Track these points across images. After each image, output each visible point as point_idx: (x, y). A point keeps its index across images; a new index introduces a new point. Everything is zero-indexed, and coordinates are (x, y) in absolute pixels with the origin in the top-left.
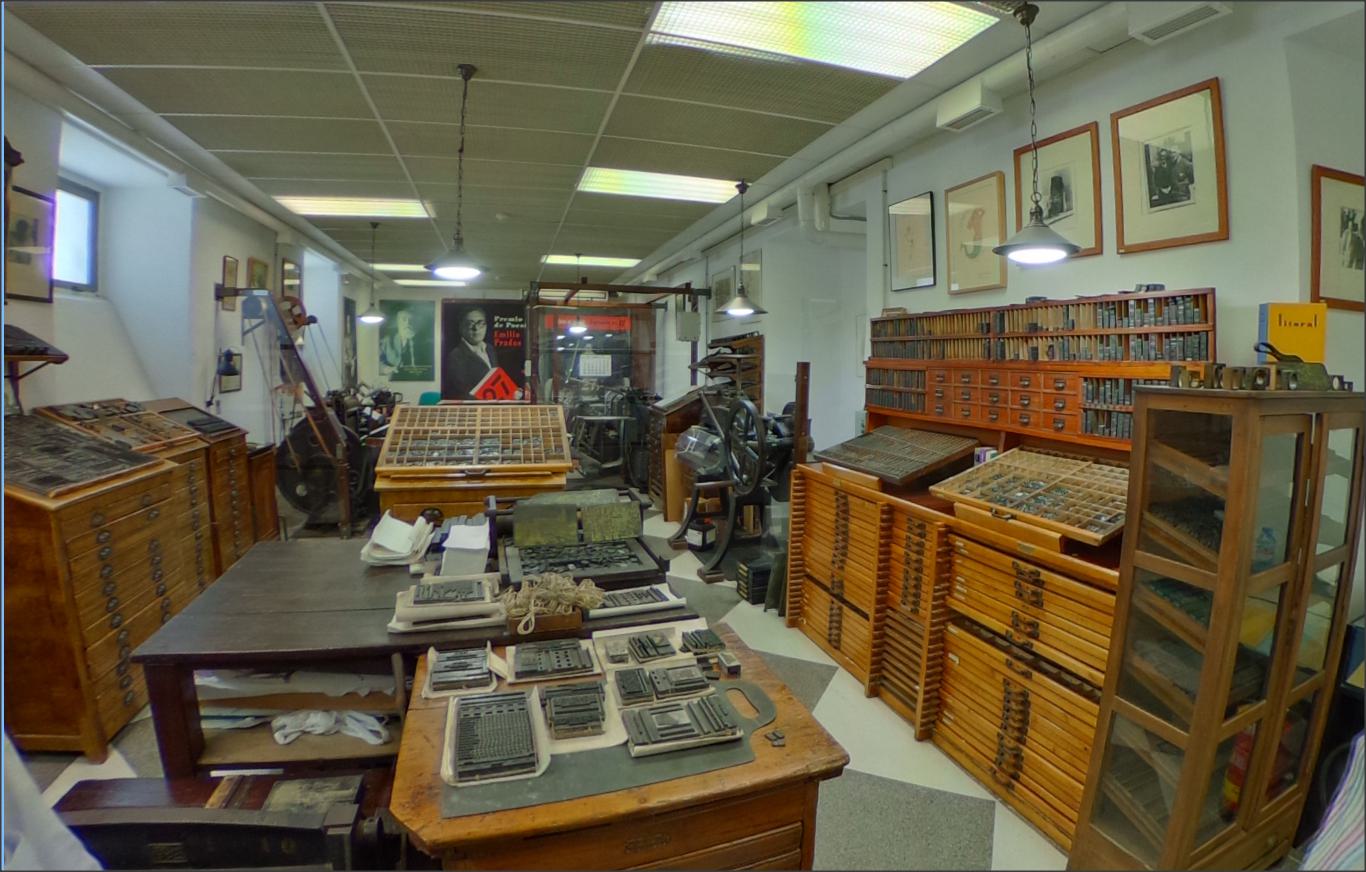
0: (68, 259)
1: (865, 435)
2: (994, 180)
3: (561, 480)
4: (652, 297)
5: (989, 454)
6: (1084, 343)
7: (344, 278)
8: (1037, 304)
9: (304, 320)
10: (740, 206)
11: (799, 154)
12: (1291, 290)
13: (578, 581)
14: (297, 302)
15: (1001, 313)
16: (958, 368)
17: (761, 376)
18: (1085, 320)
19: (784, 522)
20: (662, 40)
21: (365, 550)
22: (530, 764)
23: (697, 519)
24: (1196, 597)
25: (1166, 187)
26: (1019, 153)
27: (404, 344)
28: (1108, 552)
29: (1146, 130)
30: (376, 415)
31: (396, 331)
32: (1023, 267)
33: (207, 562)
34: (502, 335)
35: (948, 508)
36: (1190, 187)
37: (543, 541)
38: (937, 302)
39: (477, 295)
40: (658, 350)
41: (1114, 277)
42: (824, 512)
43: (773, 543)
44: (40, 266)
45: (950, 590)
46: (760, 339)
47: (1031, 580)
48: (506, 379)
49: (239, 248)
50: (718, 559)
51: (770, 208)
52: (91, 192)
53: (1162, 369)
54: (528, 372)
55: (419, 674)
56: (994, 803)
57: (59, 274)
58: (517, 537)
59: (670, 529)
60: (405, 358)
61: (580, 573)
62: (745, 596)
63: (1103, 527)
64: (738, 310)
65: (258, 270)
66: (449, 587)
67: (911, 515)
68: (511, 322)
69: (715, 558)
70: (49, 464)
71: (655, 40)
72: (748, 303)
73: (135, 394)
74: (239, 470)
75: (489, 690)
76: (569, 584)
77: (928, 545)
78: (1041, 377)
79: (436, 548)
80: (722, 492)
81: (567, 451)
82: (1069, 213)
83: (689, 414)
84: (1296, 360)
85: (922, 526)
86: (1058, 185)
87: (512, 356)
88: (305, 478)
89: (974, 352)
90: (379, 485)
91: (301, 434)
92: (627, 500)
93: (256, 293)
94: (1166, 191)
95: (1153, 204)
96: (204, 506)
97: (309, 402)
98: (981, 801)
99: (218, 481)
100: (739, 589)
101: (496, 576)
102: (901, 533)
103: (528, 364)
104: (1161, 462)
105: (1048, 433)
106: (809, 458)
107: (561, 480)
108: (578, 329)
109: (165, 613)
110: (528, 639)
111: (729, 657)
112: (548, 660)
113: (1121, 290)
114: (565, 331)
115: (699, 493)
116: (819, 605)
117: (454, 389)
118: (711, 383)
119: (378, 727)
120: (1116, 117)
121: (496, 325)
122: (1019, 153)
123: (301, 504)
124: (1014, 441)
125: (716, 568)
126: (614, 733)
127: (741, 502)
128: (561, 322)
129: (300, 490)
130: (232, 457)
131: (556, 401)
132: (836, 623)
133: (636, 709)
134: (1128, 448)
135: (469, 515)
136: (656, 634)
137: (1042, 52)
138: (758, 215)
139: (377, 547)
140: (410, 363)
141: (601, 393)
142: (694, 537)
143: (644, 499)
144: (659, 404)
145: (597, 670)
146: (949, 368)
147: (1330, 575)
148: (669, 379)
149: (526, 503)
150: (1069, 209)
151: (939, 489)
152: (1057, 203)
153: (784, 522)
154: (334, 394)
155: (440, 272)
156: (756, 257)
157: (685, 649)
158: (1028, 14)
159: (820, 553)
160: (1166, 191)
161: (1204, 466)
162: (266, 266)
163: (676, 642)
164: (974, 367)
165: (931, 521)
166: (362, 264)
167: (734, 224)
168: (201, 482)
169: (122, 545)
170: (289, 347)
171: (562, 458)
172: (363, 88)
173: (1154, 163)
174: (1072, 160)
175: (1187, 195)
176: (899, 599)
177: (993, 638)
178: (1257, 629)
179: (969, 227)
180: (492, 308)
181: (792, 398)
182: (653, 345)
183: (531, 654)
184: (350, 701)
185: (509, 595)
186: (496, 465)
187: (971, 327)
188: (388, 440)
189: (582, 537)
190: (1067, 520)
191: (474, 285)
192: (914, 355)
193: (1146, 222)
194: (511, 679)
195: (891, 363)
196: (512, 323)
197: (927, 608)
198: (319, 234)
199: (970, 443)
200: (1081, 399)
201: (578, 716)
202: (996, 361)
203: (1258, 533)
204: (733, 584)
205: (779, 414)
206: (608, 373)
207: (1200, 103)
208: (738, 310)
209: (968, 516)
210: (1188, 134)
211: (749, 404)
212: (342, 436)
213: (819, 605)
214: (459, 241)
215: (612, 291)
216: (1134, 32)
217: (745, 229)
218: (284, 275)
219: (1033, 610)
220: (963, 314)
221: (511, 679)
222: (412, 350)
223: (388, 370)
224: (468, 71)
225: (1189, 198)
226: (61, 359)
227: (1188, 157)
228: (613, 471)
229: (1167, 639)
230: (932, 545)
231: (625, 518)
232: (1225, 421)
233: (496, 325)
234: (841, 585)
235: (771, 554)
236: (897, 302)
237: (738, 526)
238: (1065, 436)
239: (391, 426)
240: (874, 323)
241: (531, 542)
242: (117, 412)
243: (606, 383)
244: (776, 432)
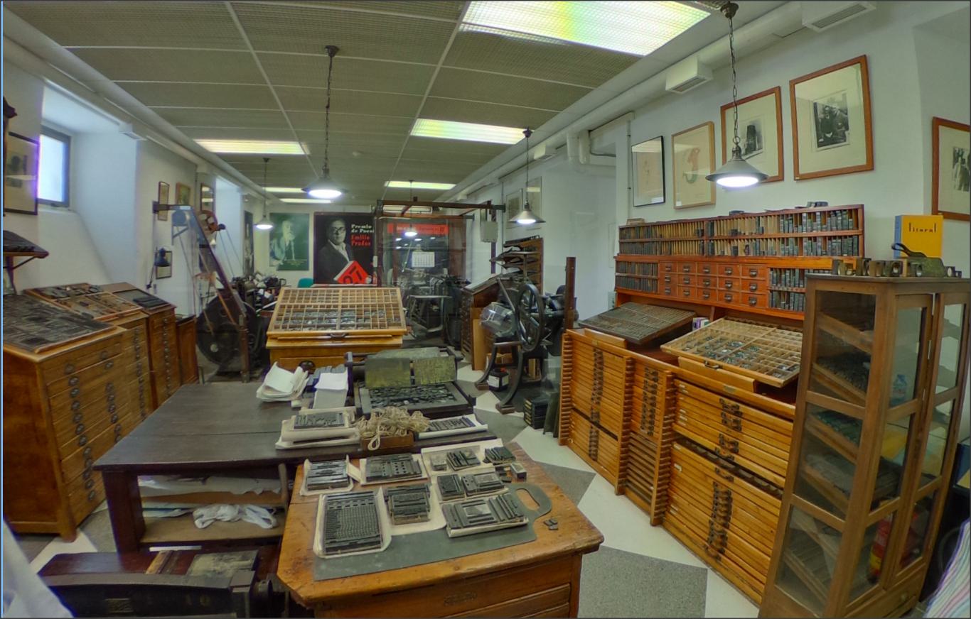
0: (48, 184)
1: (615, 308)
2: (706, 128)
3: (399, 341)
4: (464, 210)
5: (703, 322)
6: (770, 244)
7: (244, 197)
8: (737, 215)
9: (216, 227)
12: (918, 206)
13: (411, 412)
14: (211, 214)
15: (712, 222)
16: (681, 261)
17: (541, 267)
18: (771, 227)
19: (557, 371)
20: (471, 28)
21: (260, 390)
22: (377, 542)
23: (496, 369)
25: (829, 133)
26: (724, 108)
27: (287, 244)
28: (788, 392)
29: (815, 92)
30: (267, 295)
31: (282, 235)
32: (727, 190)
33: (147, 399)
34: (357, 238)
35: (674, 360)
36: (846, 133)
37: (386, 384)
38: (666, 214)
39: (339, 210)
40: (468, 248)
41: (792, 197)
42: (586, 363)
43: (550, 385)
44: (29, 189)
45: (675, 419)
46: (540, 240)
47: (733, 412)
48: (360, 269)
49: (170, 176)
50: (510, 397)
52: (65, 136)
53: (826, 262)
54: (375, 264)
55: (298, 478)
56: (706, 570)
57: (42, 194)
58: (368, 381)
59: (476, 376)
60: (288, 254)
61: (412, 406)
62: (530, 423)
63: (784, 374)
64: (524, 220)
65: (183, 192)
66: (319, 417)
67: (648, 366)
68: (363, 229)
69: (509, 396)
70: (35, 329)
71: (466, 28)
72: (531, 215)
73: (96, 280)
74: (170, 333)
75: (348, 490)
76: (404, 414)
77: (659, 387)
78: (740, 268)
79: (310, 389)
80: (513, 350)
81: (403, 320)
82: (760, 151)
83: (490, 294)
84: (921, 255)
85: (655, 373)
86: (752, 131)
87: (364, 253)
88: (217, 340)
89: (692, 250)
90: (269, 344)
91: (214, 308)
92: (446, 355)
94: (829, 135)
95: (820, 145)
96: (145, 359)
97: (219, 285)
98: (698, 569)
99: (155, 341)
100: (525, 418)
101: (353, 409)
102: (641, 378)
103: (375, 258)
104: (825, 328)
105: (745, 307)
106: (575, 325)
107: (399, 341)
108: (411, 234)
109: (117, 435)
110: (375, 453)
111: (518, 466)
112: (390, 469)
113: (797, 206)
114: (402, 235)
115: (497, 350)
116: (582, 430)
117: (323, 276)
118: (505, 272)
119: (268, 516)
120: (793, 83)
121: (353, 231)
122: (724, 108)
123: (214, 357)
124: (721, 313)
125: (509, 403)
126: (437, 520)
127: (527, 357)
128: (399, 228)
129: (214, 348)
130: (165, 324)
131: (395, 284)
132: (594, 442)
133: (452, 503)
134: (802, 318)
135: (334, 365)
136: (466, 450)
137: (740, 37)
138: (539, 152)
139: (268, 388)
140: (292, 258)
141: (427, 279)
142: (493, 381)
143: (458, 354)
144: (469, 287)
145: (424, 476)
146: (675, 261)
148: (475, 269)
149: (374, 357)
150: (760, 148)
151: (668, 347)
152: (751, 144)
153: (557, 371)
154: (237, 279)
155: (313, 193)
156: (538, 182)
157: (487, 461)
158: (731, 10)
159: (583, 392)
160: (829, 135)
161: (856, 331)
163: (481, 456)
165: (661, 369)
166: (258, 187)
167: (522, 159)
168: (143, 342)
169: (87, 387)
170: (205, 246)
171: (399, 325)
172: (258, 63)
173: (821, 116)
174: (762, 113)
175: (844, 138)
176: (639, 425)
177: (706, 453)
179: (689, 161)
180: (349, 219)
181: (563, 283)
182: (464, 245)
183: (377, 464)
184: (249, 498)
185: (362, 422)
186: (353, 330)
187: (691, 232)
188: (275, 312)
189: (413, 382)
190: (758, 369)
191: (337, 202)
192: (650, 252)
193: (814, 157)
194: (363, 482)
195: (633, 257)
196: (364, 229)
197: (659, 432)
198: (227, 166)
199: (690, 314)
200: (768, 283)
201: (411, 508)
202: (708, 257)
203: (894, 378)
204: (521, 415)
205: (554, 294)
206: (432, 265)
208: (524, 220)
209: (688, 366)
210: (844, 95)
211: (533, 287)
212: (243, 310)
213: (582, 430)
214: (326, 171)
215: (435, 207)
217: (530, 163)
218: (202, 195)
219: (734, 433)
220: (684, 223)
221: (363, 482)
222: (293, 248)
223: (276, 263)
224: (333, 51)
225: (845, 141)
226: (43, 255)
227: (845, 111)
228: (436, 335)
230: (662, 387)
231: (445, 368)
232: (871, 299)
233: (353, 231)
234: (598, 415)
235: (548, 393)
236: (638, 214)
237: (525, 373)
238: (757, 310)
239: (278, 303)
240: (622, 229)
241: (377, 385)
242: (83, 292)
243: (431, 272)
244: (552, 306)
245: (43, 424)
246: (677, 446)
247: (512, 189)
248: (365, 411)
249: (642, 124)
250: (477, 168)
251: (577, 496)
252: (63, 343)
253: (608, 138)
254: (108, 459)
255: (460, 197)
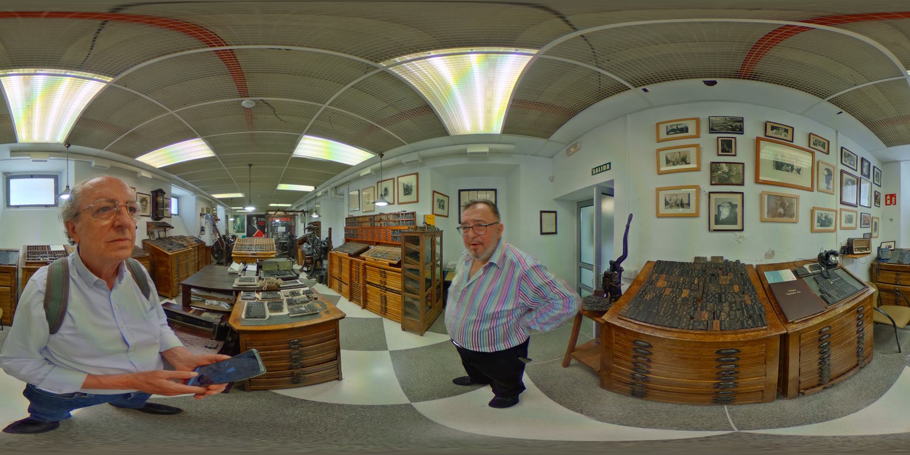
0: (174, 210)
1: (345, 244)
2: (372, 188)
3: (274, 256)
4: (295, 213)
5: (372, 247)
6: (391, 222)
7: (225, 211)
8: (381, 214)
9: (217, 220)
10: (315, 192)
11: (329, 180)
12: (429, 212)
13: (277, 279)
14: (216, 216)
15: (374, 216)
16: (365, 228)
17: (320, 231)
18: (391, 218)
19: (327, 265)
20: (296, 156)
21: (229, 269)
22: (264, 317)
23: (306, 265)
24: (416, 271)
26: (378, 182)
28: (399, 265)
29: (403, 180)
30: (232, 240)
31: (237, 222)
32: (378, 206)
33: (196, 268)
35: (364, 259)
37: (269, 269)
38: (360, 214)
39: (254, 213)
40: (296, 225)
41: (397, 209)
42: (336, 262)
43: (324, 270)
44: (169, 211)
45: (366, 277)
46: (320, 222)
47: (383, 273)
49: (203, 205)
50: (311, 274)
51: (322, 192)
52: (177, 197)
53: (406, 228)
54: (266, 231)
55: (239, 296)
57: (172, 213)
58: (263, 268)
59: (300, 267)
60: (239, 228)
61: (278, 277)
63: (397, 260)
64: (315, 216)
65: (208, 210)
66: (247, 278)
67: (356, 261)
68: (262, 219)
69: (310, 274)
70: (170, 247)
71: (294, 156)
72: (317, 214)
73: (185, 235)
74: (204, 250)
75: (255, 301)
76: (275, 279)
77: (360, 268)
78: (382, 230)
79: (245, 270)
80: (312, 258)
81: (275, 249)
83: (304, 240)
84: (430, 225)
85: (359, 264)
86: (386, 190)
87: (262, 227)
88: (217, 253)
89: (368, 225)
90: (233, 255)
91: (216, 244)
92: (289, 260)
93: (208, 214)
95: (404, 195)
96: (197, 257)
97: (218, 237)
99: (200, 252)
100: (316, 280)
101: (258, 277)
102: (354, 266)
103: (266, 229)
104: (408, 246)
105: (384, 242)
106: (332, 250)
107: (274, 256)
108: (277, 221)
109: (187, 277)
110: (265, 291)
111: (315, 295)
112: (270, 296)
114: (275, 221)
115: (306, 259)
116: (336, 283)
117: (249, 235)
118: (309, 233)
119: (228, 306)
120: (398, 177)
122: (378, 182)
123: (216, 258)
124: (378, 244)
125: (311, 276)
126: (286, 311)
127: (316, 260)
128: (274, 219)
129: (216, 255)
130: (202, 248)
131: (272, 237)
132: (340, 287)
133: (291, 307)
134: (401, 244)
135: (252, 263)
136: (297, 290)
137: (384, 163)
138: (319, 194)
139: (231, 269)
141: (283, 235)
142: (305, 269)
143: (293, 260)
144: (297, 238)
145: (282, 298)
146: (363, 228)
147: (439, 263)
148: (299, 232)
149: (266, 261)
151: (362, 255)
153: (327, 265)
154: (224, 235)
155: (246, 208)
156: (319, 203)
157: (303, 294)
158: (382, 155)
159: (336, 271)
161: (415, 246)
162: (210, 209)
163: (301, 292)
164: (369, 228)
165: (361, 262)
166: (229, 207)
167: (314, 196)
168: (196, 252)
169: (181, 263)
170: (214, 225)
171: (274, 251)
173: (405, 187)
174: (389, 185)
175: (411, 193)
176: (354, 280)
177: (376, 286)
178: (428, 275)
180: (258, 216)
181: (328, 236)
182: (295, 224)
183: (265, 294)
184: (223, 300)
185: (261, 281)
186: (259, 252)
187: (368, 219)
188: (235, 246)
189: (278, 269)
190: (390, 259)
191: (254, 211)
192: (355, 226)
193: (403, 198)
194: (260, 299)
195: (350, 227)
197: (361, 282)
198: (220, 201)
199: (368, 245)
200: (391, 234)
201: (277, 307)
202: (373, 227)
203: (426, 258)
204: (315, 279)
205: (325, 240)
206: (285, 231)
207: (414, 177)
208: (315, 216)
209: (369, 261)
211: (318, 238)
212: (225, 244)
213: (336, 283)
214: (250, 202)
215: (285, 212)
216: (403, 162)
217: (316, 197)
218: (213, 211)
219: (385, 279)
220: (365, 216)
221: (260, 299)
223: (235, 230)
224: (250, 165)
226: (173, 228)
227: (411, 186)
228: (286, 254)
229: (412, 280)
230: (361, 268)
231: (289, 265)
232: (418, 237)
234: (341, 278)
235: (324, 272)
236: (351, 214)
237: (316, 266)
238: (388, 242)
239: (236, 243)
240: (346, 218)
241: (266, 270)
242: (182, 238)
243: (284, 233)
244: (324, 244)
245: (170, 271)
246: (367, 285)
247: (310, 206)
248: (262, 278)
249: (352, 186)
250: (298, 199)
251: (336, 303)
252: (177, 251)
253: (343, 190)
254: (184, 282)
255: (294, 209)
